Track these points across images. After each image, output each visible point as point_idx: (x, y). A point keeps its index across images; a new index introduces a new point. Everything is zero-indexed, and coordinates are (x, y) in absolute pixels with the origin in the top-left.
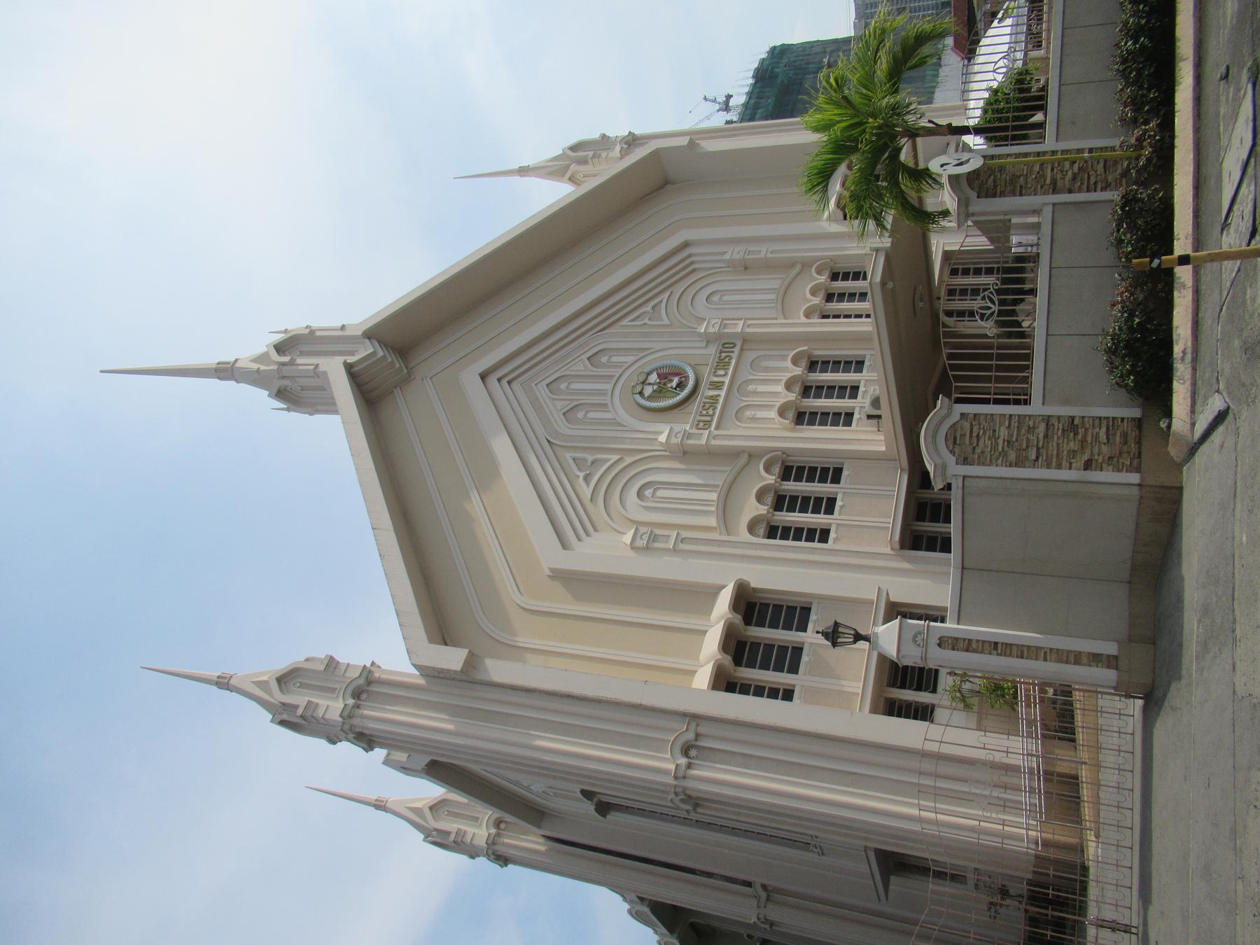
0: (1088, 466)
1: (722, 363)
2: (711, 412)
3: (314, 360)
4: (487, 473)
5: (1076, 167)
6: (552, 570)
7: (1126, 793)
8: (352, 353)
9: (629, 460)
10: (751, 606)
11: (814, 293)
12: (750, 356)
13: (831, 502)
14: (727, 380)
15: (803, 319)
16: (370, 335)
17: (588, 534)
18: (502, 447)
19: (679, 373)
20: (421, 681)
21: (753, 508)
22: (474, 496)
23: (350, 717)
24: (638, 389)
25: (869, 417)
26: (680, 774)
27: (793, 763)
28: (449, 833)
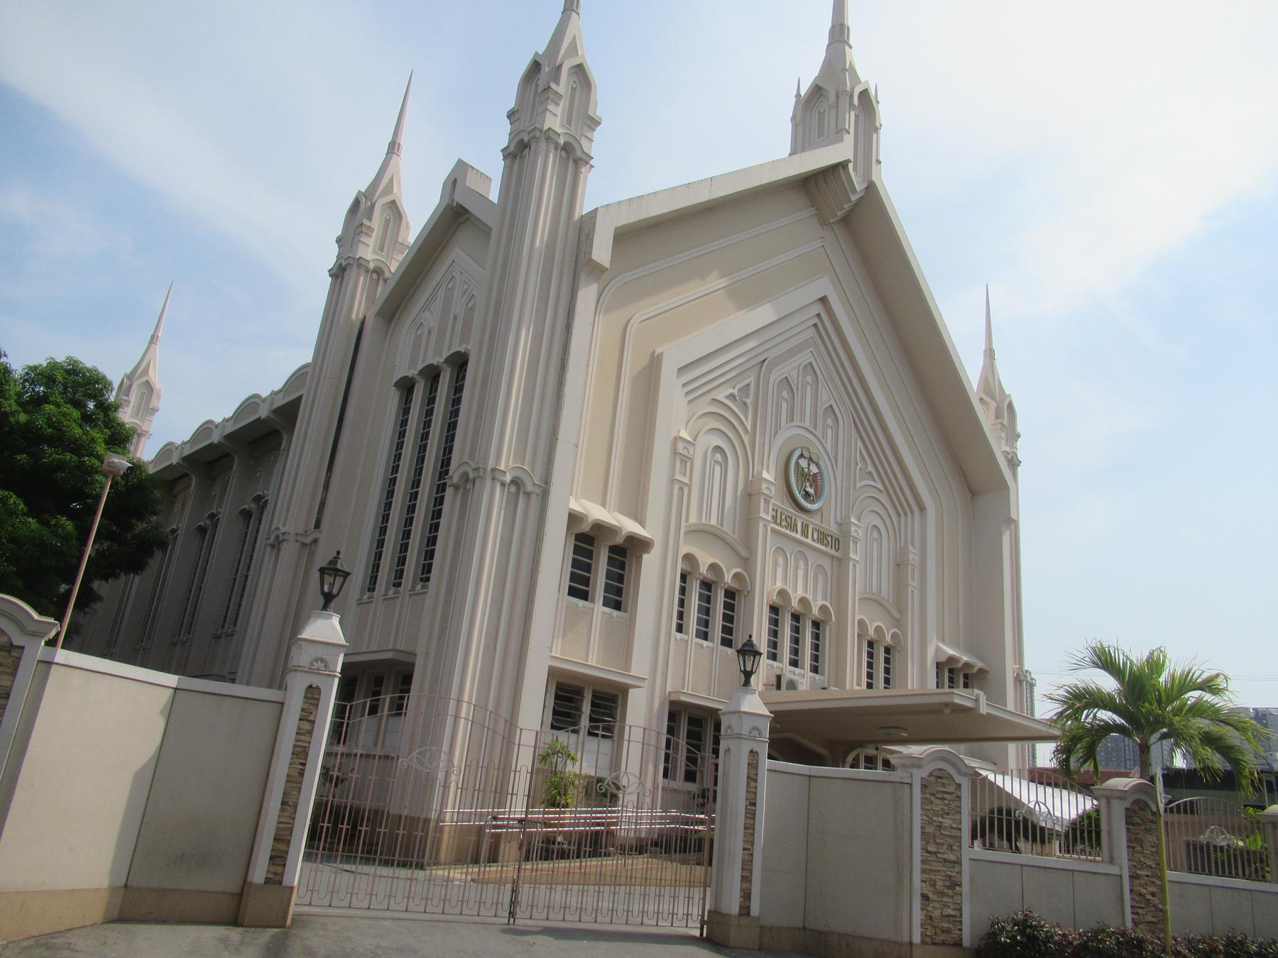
0: (925, 897)
1: (823, 537)
2: (784, 523)
3: (852, 130)
4: (744, 297)
5: (1149, 897)
6: (661, 355)
7: (639, 920)
8: (855, 169)
9: (746, 439)
10: (626, 553)
11: (878, 629)
12: (827, 564)
13: (705, 636)
14: (809, 541)
15: (858, 617)
16: (871, 189)
17: (687, 393)
18: (764, 314)
19: (818, 494)
20: (576, 217)
21: (705, 560)
22: (723, 282)
23: (548, 139)
24: (806, 454)
25: (779, 678)
26: (498, 476)
27: (504, 586)
28: (370, 219)
